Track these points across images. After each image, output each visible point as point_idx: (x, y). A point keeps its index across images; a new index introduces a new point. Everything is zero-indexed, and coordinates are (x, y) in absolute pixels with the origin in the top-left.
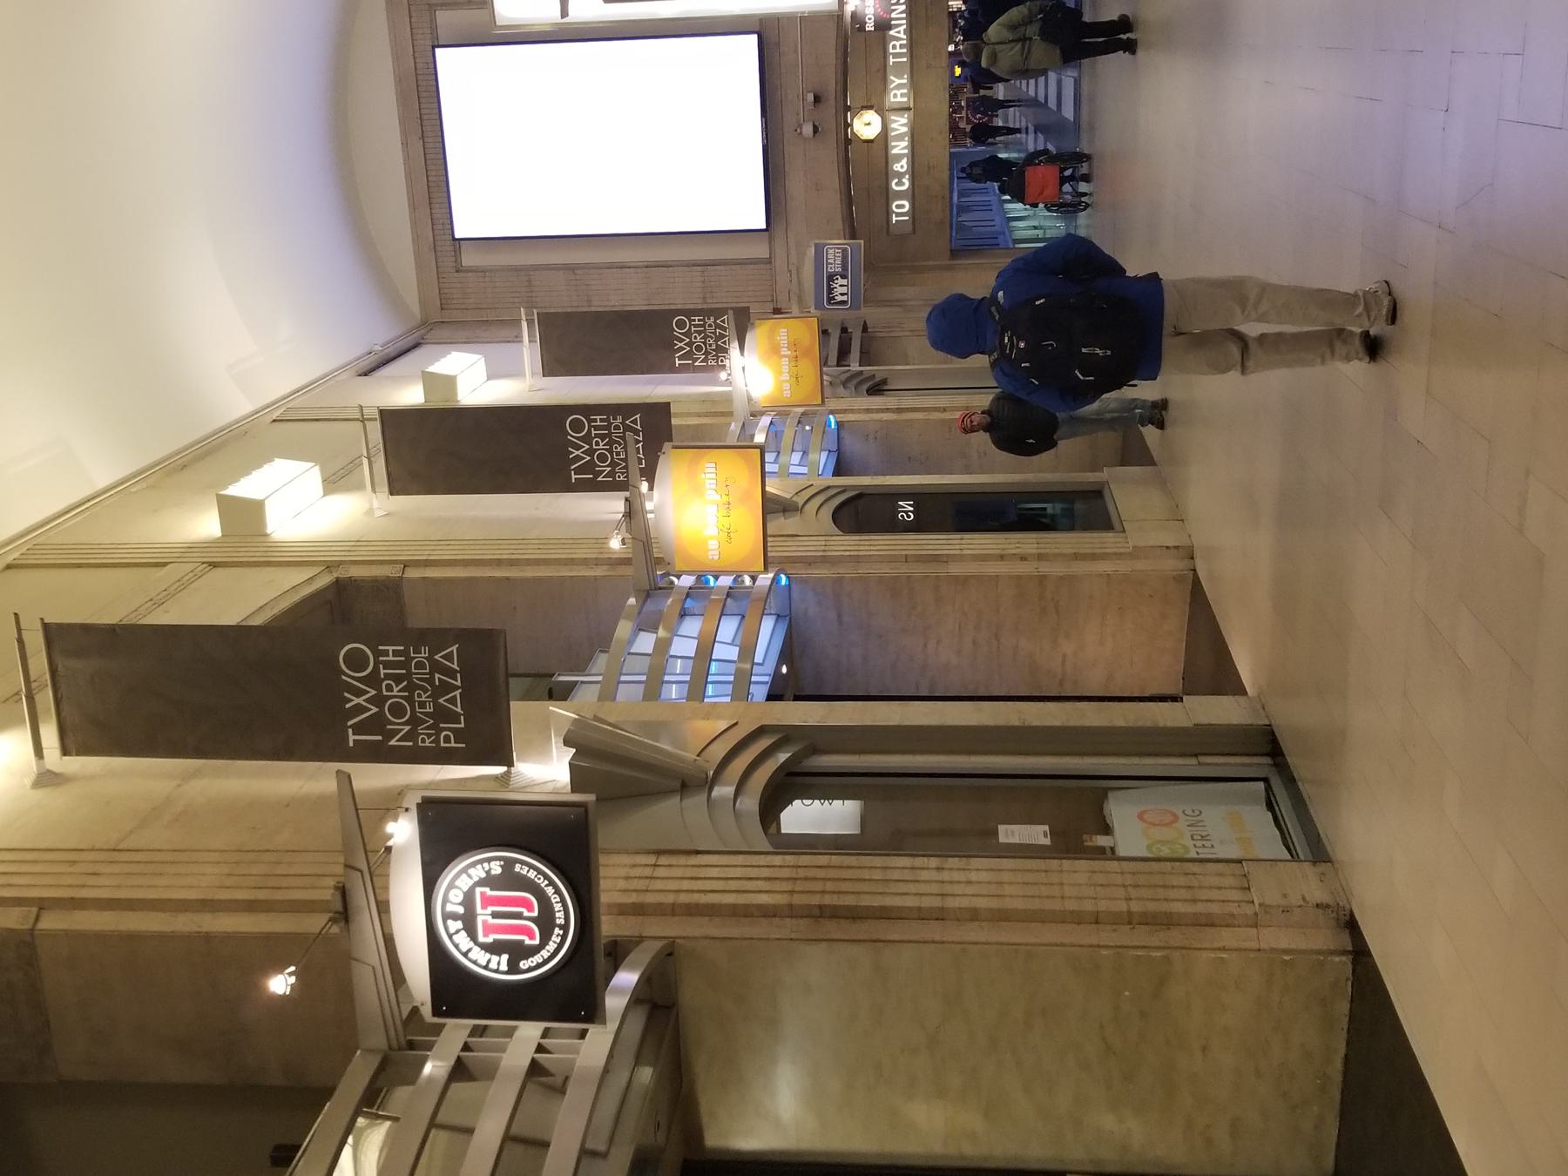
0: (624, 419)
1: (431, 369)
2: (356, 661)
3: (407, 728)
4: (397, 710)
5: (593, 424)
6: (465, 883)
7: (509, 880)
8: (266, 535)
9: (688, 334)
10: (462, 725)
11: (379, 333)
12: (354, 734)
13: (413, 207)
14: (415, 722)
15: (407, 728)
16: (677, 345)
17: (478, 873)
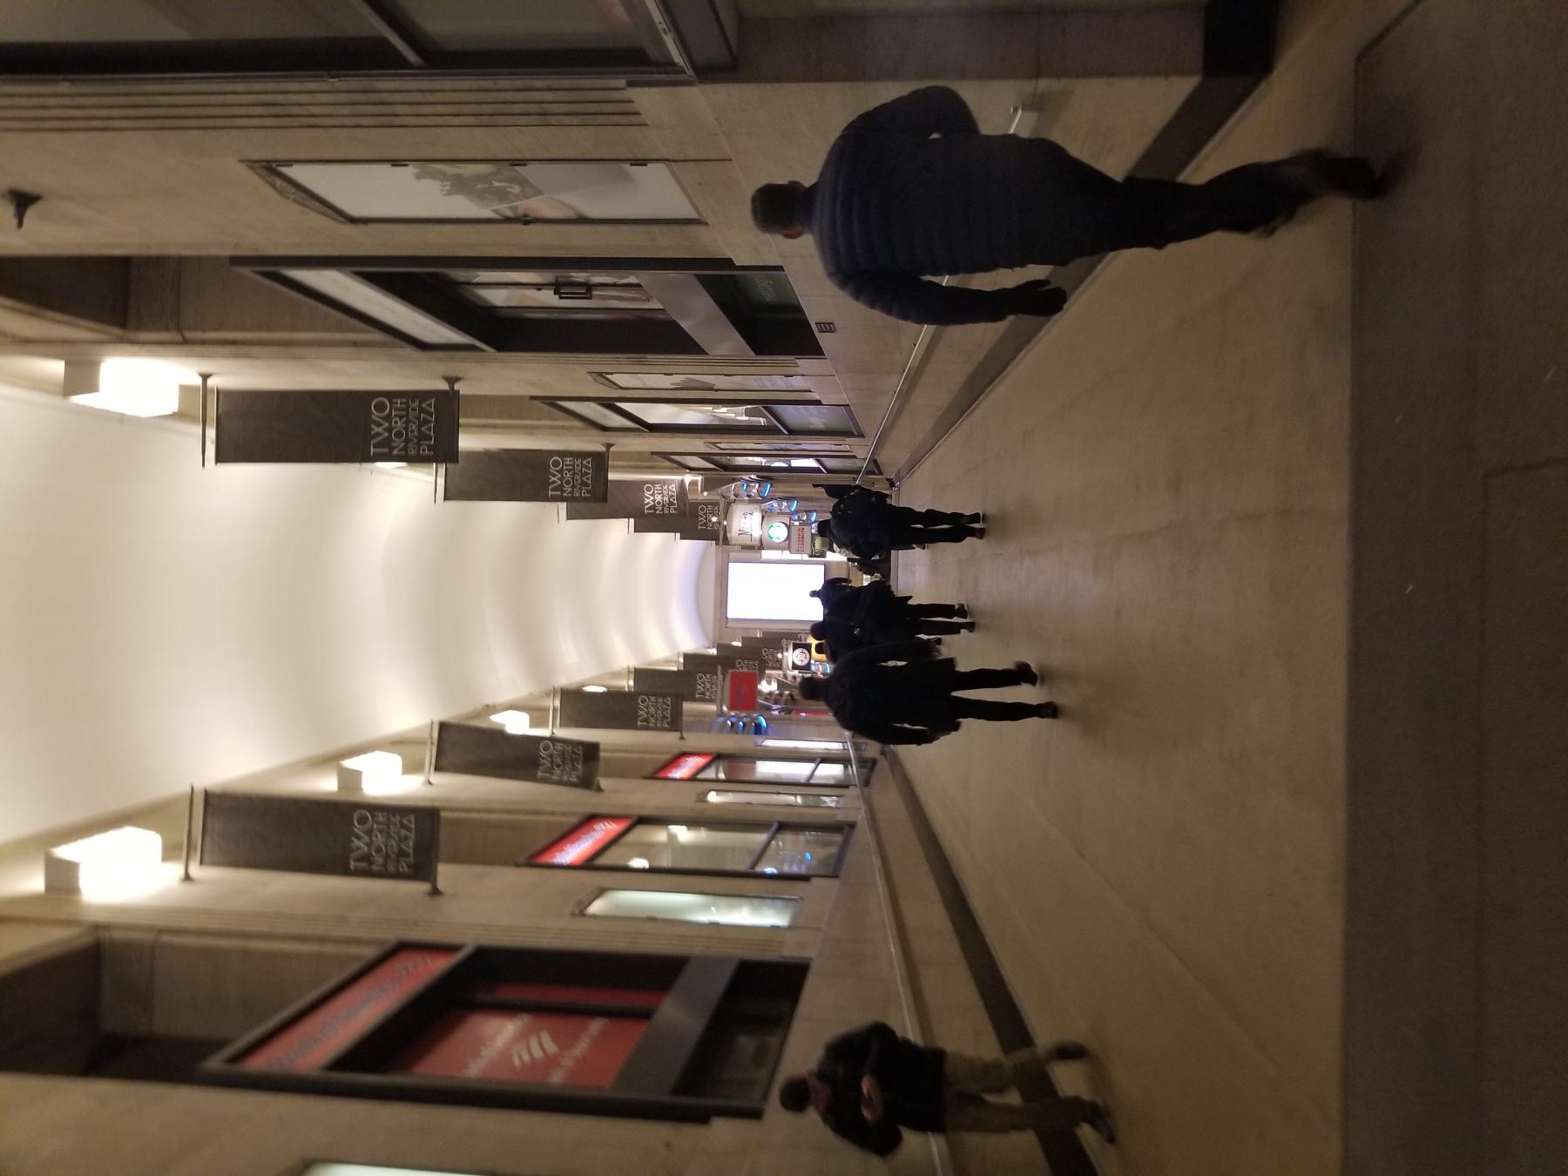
11: (707, 644)
13: (715, 607)
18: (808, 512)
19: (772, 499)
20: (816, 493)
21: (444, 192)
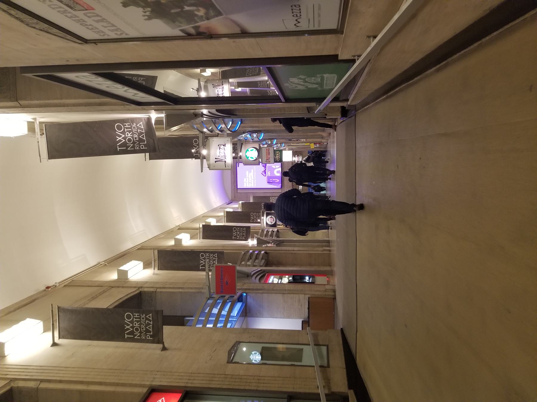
0: (146, 315)
1: (119, 269)
2: (252, 214)
3: (139, 334)
4: (238, 235)
5: (134, 316)
6: (269, 218)
7: (271, 217)
8: (182, 245)
9: (272, 199)
10: (152, 334)
12: (127, 335)
14: (141, 332)
15: (139, 334)
16: (126, 327)
17: (269, 217)
18: (271, 139)
19: (244, 133)
20: (275, 126)
21: (146, 17)
